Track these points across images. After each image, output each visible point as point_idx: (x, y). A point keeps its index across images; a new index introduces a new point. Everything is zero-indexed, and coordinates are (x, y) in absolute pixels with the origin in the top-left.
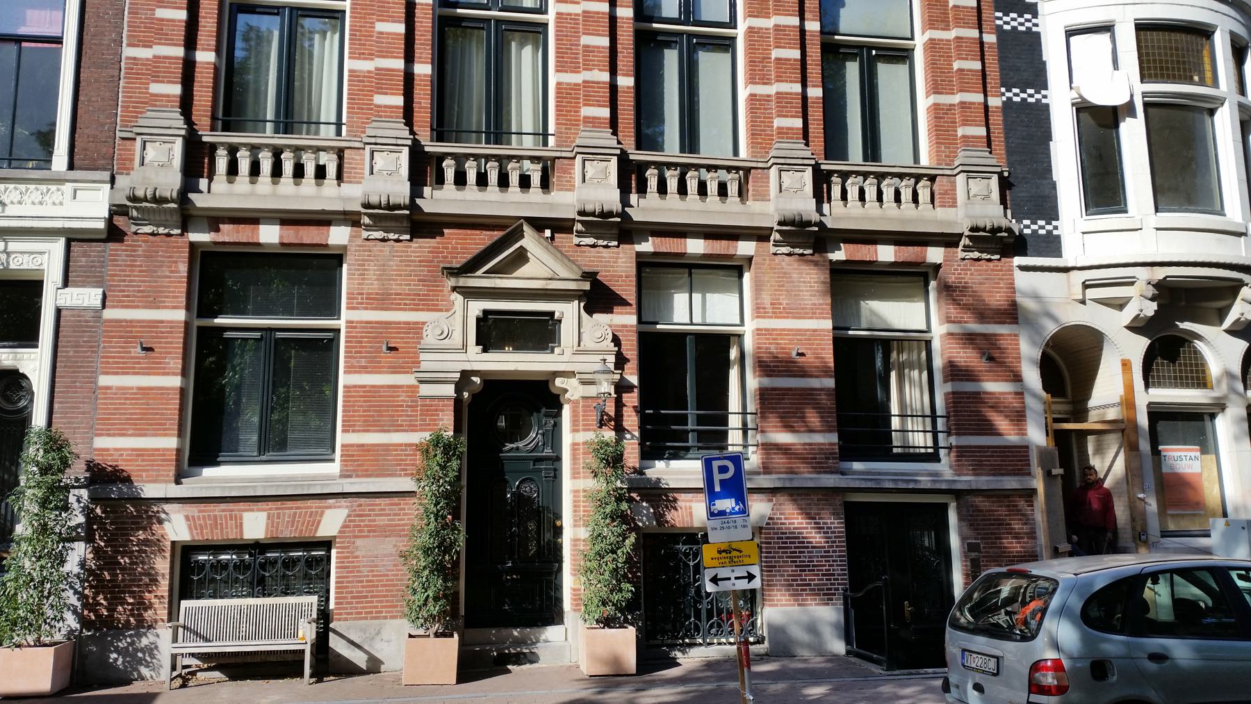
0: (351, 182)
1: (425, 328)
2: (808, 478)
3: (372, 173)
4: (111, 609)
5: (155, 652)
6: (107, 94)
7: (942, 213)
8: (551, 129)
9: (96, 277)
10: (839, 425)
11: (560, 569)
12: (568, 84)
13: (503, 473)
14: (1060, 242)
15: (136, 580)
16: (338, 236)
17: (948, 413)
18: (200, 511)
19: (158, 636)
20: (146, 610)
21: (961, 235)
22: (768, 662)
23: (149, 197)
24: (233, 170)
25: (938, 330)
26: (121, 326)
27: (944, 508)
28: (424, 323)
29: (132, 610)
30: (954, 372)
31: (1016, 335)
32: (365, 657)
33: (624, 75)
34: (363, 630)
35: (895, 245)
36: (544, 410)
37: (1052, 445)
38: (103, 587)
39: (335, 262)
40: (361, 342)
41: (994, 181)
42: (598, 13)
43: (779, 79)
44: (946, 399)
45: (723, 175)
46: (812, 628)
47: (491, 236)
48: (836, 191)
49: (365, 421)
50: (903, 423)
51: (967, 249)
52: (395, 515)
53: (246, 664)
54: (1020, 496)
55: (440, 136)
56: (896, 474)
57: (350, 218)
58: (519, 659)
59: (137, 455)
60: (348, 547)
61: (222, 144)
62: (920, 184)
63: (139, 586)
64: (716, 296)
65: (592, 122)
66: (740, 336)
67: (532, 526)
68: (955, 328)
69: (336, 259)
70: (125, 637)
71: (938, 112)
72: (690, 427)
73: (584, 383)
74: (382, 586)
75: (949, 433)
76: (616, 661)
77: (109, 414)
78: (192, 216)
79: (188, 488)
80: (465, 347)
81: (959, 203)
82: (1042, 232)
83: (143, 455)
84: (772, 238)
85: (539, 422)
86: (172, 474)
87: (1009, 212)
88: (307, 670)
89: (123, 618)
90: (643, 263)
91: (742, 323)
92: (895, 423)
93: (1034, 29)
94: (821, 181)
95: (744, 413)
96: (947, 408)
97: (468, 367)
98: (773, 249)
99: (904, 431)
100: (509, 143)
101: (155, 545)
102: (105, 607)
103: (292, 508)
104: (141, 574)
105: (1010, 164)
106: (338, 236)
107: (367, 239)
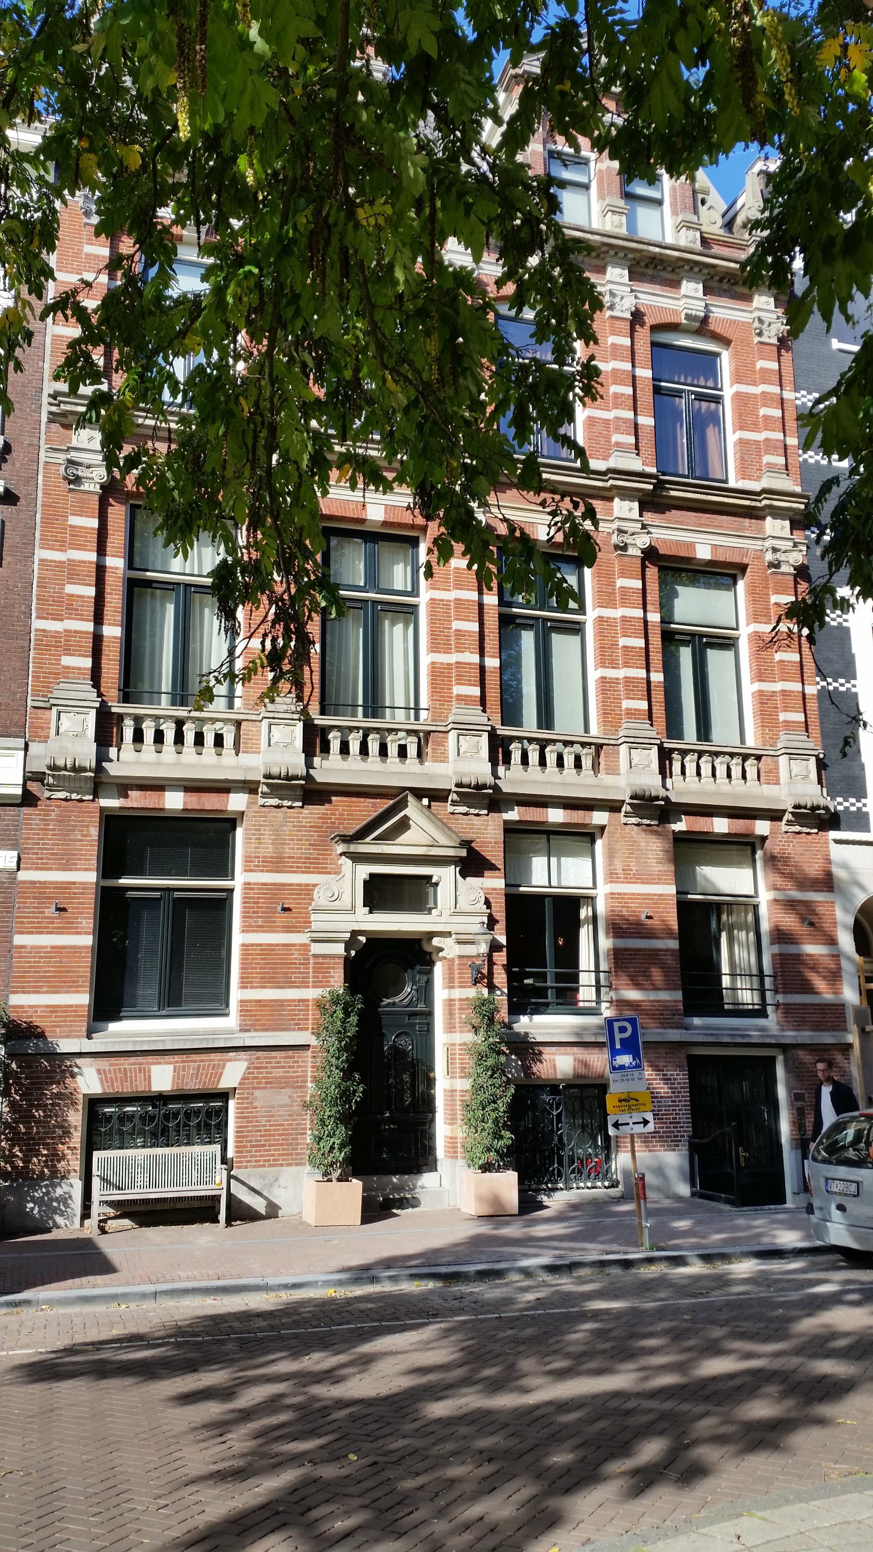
0: (247, 752)
1: (317, 890)
2: (653, 1033)
3: (58, 733)
4: (27, 1161)
5: (69, 1201)
6: (18, 665)
7: (767, 790)
8: (424, 703)
9: (10, 840)
10: (683, 984)
11: (433, 1120)
12: (442, 664)
13: (380, 1027)
14: (868, 819)
15: (49, 1132)
16: (236, 802)
17: (775, 973)
18: (111, 1065)
19: (71, 1186)
20: (59, 1161)
21: (784, 811)
22: (625, 1203)
23: (69, 766)
24: (138, 737)
25: (765, 898)
26: (35, 888)
27: (772, 1060)
28: (315, 885)
29: (46, 1161)
30: (780, 936)
31: (833, 902)
32: (265, 1202)
33: (490, 656)
34: (263, 1177)
35: (564, 808)
36: (418, 967)
37: (865, 1003)
38: (19, 1139)
39: (228, 825)
40: (257, 903)
41: (812, 763)
42: (468, 601)
43: (626, 665)
44: (773, 960)
45: (577, 748)
46: (659, 1171)
47: (374, 805)
48: (676, 767)
49: (262, 978)
50: (733, 981)
51: (789, 823)
52: (290, 1067)
53: (151, 1212)
54: (838, 1050)
55: (126, 698)
56: (732, 1029)
57: (250, 787)
58: (403, 1203)
59: (51, 1012)
60: (247, 1098)
61: (129, 715)
62: (703, 759)
63: (53, 1138)
64: (570, 860)
65: (463, 699)
66: (591, 900)
67: (406, 1077)
68: (780, 896)
69: (231, 822)
70: (41, 1187)
71: (762, 698)
72: (549, 984)
73: (459, 942)
74: (279, 1135)
75: (776, 991)
76: (496, 1201)
77: (25, 972)
78: (102, 783)
79: (97, 1044)
80: (353, 908)
81: (782, 781)
82: (853, 809)
83: (56, 1012)
84: (450, 798)
85: (413, 978)
86: (84, 1029)
87: (825, 790)
88: (222, 1216)
89: (37, 1169)
90: (511, 830)
91: (595, 886)
92: (726, 981)
93: (845, 624)
94: (665, 755)
95: (597, 971)
96: (774, 968)
97: (357, 927)
98: (624, 820)
99: (734, 989)
100: (383, 717)
101: (69, 1098)
102: (21, 1159)
103: (196, 1061)
104: (54, 1126)
105: (825, 747)
106: (236, 802)
107: (263, 806)
